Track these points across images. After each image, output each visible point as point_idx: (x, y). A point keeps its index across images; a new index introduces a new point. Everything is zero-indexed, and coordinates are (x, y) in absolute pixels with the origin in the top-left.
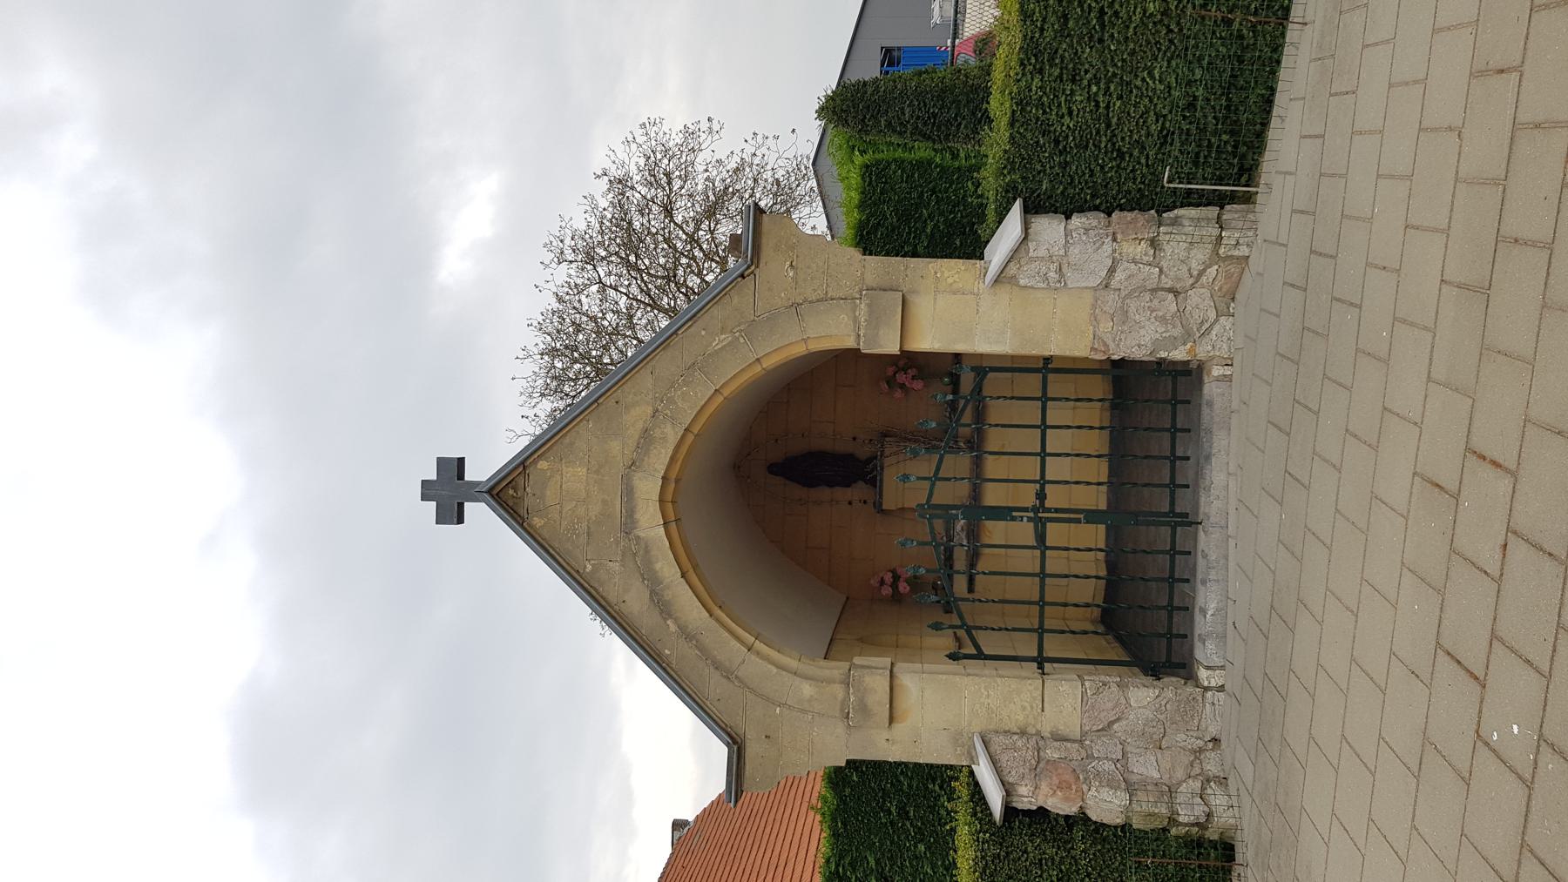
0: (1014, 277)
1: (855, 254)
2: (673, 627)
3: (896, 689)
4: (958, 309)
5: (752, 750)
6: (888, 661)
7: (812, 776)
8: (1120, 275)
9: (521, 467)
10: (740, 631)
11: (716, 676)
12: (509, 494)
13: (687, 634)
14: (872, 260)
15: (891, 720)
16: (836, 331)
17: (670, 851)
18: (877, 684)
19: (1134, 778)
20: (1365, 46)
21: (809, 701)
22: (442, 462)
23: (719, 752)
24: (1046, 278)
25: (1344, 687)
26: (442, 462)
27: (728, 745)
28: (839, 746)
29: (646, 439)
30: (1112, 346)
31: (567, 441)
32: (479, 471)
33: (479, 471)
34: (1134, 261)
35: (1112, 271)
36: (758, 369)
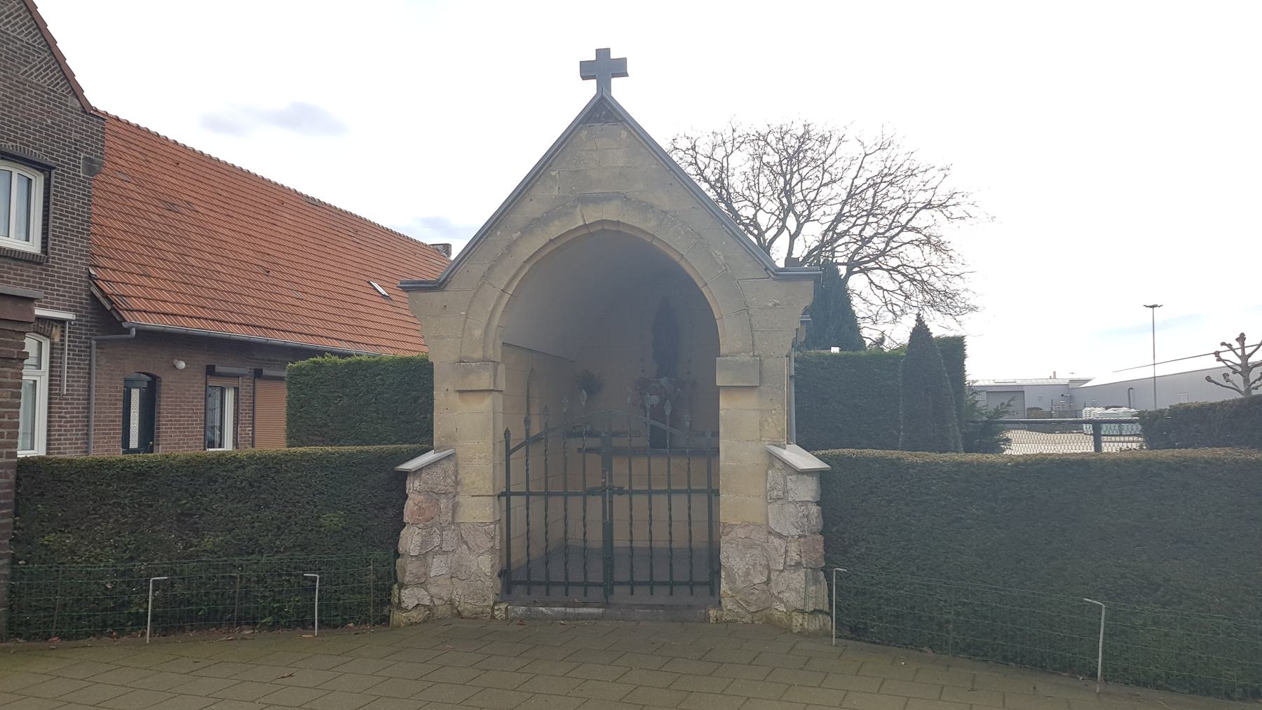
6: (502, 385)
10: (515, 283)
12: (602, 113)
15: (460, 392)
16: (730, 339)
19: (429, 559)
24: (773, 489)
28: (442, 358)
32: (620, 90)
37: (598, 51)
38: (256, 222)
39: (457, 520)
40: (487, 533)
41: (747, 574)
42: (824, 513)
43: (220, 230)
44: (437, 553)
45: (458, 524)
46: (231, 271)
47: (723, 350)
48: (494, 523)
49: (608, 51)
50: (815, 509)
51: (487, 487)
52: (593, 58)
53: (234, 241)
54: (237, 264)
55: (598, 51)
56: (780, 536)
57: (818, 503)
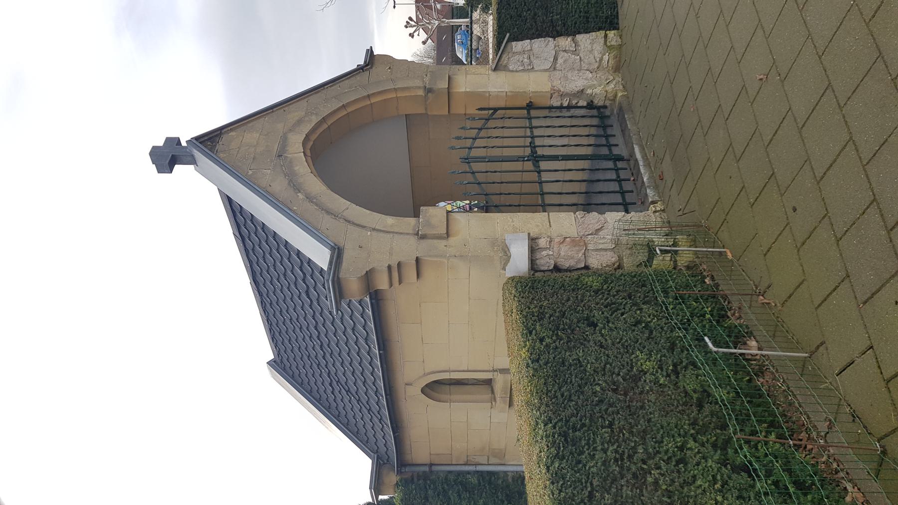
0: (506, 66)
3: (450, 221)
5: (347, 256)
8: (560, 61)
11: (327, 218)
13: (309, 198)
17: (370, 461)
29: (300, 122)
31: (250, 125)
34: (565, 51)
35: (556, 59)
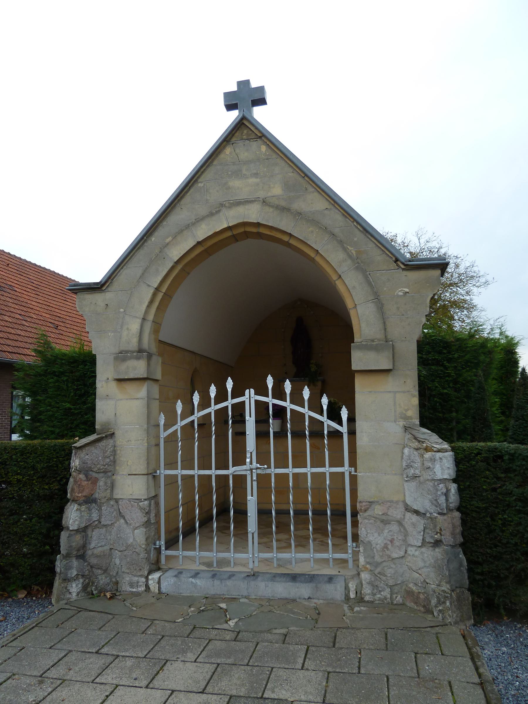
1: (417, 334)
2: (168, 240)
4: (385, 405)
6: (159, 376)
7: (82, 322)
9: (262, 136)
10: (168, 282)
12: (244, 130)
14: (414, 347)
15: (119, 380)
16: (365, 321)
18: (138, 367)
19: (89, 532)
20: (419, 677)
21: (128, 329)
22: (261, 89)
23: (96, 276)
24: (409, 466)
25: (61, 681)
26: (261, 89)
27: (101, 282)
28: (103, 348)
30: (366, 514)
32: (259, 113)
33: (259, 113)
36: (334, 277)
37: (239, 84)
38: (54, 299)
39: (115, 497)
40: (141, 509)
41: (386, 547)
42: (460, 491)
43: (29, 302)
44: (96, 527)
45: (117, 501)
46: (32, 325)
47: (356, 340)
48: (150, 499)
49: (247, 82)
50: (453, 487)
51: (142, 468)
52: (235, 88)
53: (38, 308)
54: (37, 321)
55: (239, 84)
56: (417, 512)
57: (454, 481)
